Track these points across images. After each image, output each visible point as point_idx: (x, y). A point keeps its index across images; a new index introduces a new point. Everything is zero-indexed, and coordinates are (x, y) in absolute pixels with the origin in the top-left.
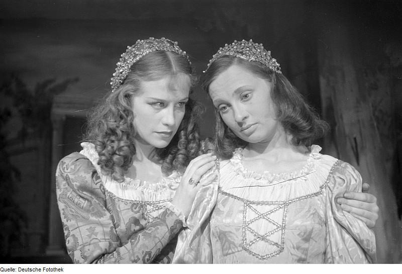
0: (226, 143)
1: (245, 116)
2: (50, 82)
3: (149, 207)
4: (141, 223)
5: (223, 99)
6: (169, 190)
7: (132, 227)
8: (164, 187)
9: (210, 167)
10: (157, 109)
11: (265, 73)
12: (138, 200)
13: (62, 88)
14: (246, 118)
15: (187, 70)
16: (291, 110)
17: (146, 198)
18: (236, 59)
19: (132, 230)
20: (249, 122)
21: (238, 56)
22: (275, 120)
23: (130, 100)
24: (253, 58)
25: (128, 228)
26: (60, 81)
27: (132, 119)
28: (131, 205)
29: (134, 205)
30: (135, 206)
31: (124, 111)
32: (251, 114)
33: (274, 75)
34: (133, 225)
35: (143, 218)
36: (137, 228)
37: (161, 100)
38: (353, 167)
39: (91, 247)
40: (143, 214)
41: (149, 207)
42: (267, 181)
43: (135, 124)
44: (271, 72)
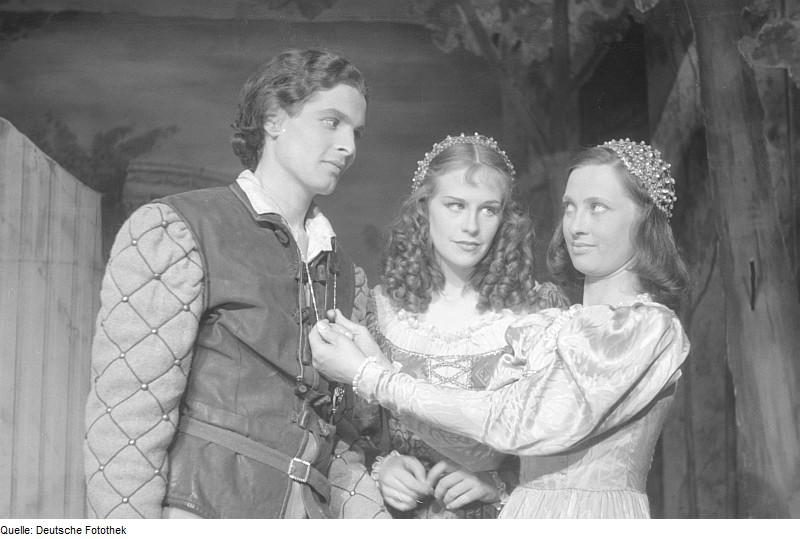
0: (558, 254)
1: (583, 230)
2: (123, 131)
10: (456, 212)
11: (641, 197)
13: (146, 143)
14: (582, 233)
16: (649, 263)
18: (617, 162)
20: (583, 240)
21: (623, 159)
23: (427, 208)
24: (638, 172)
26: (141, 131)
27: (428, 230)
31: (418, 220)
33: (651, 207)
37: (460, 200)
38: (49, 158)
42: (105, 317)
44: (648, 200)
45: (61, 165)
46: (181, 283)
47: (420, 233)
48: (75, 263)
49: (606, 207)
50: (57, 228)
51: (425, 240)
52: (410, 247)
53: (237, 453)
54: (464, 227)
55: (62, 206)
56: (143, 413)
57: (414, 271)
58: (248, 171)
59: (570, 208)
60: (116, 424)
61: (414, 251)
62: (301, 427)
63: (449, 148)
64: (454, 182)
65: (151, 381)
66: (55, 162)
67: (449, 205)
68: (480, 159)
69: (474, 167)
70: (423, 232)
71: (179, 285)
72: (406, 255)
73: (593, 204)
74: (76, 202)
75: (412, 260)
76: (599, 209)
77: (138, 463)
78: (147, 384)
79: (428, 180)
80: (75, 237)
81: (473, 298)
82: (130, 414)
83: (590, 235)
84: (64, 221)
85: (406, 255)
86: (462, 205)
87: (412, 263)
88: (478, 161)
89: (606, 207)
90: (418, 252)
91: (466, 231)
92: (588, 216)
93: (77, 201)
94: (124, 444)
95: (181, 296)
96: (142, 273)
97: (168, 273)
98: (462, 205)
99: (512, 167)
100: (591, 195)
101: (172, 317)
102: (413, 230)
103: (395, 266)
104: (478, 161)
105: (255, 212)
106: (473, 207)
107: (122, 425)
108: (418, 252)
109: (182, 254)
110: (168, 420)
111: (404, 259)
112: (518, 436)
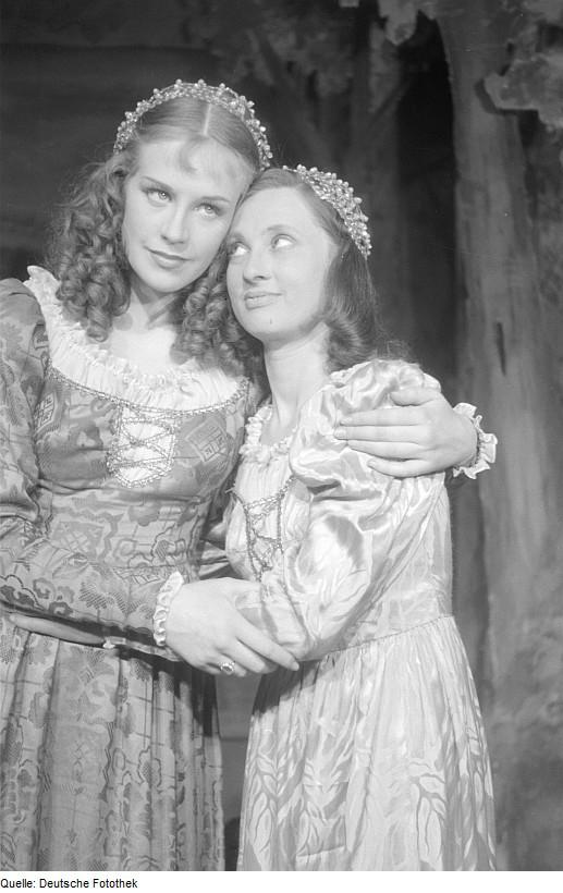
3: (126, 412)
4: (101, 437)
5: (288, 345)
6: (176, 393)
7: (80, 437)
8: (170, 384)
9: (390, 492)
12: (109, 392)
15: (227, 133)
17: (128, 395)
19: (80, 443)
22: (59, 305)
25: (73, 437)
27: (121, 220)
28: (92, 398)
29: (99, 399)
30: (100, 403)
32: (276, 277)
34: (83, 434)
35: (109, 428)
36: (91, 443)
39: (194, 346)
40: (111, 421)
41: (126, 412)
43: (330, 256)
47: (111, 224)
51: (119, 236)
52: (97, 242)
54: (164, 230)
57: (103, 280)
61: (103, 248)
63: (171, 100)
64: (161, 157)
67: (149, 191)
68: (209, 131)
69: (197, 139)
70: (115, 223)
72: (90, 251)
75: (101, 260)
76: (283, 243)
79: (130, 147)
81: (165, 336)
85: (90, 251)
86: (166, 192)
87: (100, 266)
88: (205, 132)
90: (109, 250)
91: (165, 238)
98: (166, 192)
99: (267, 148)
100: (273, 223)
102: (102, 217)
103: (73, 264)
104: (205, 132)
106: (183, 202)
108: (109, 250)
110: (247, 449)
111: (87, 256)
112: (285, 596)
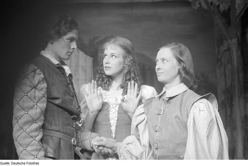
1: (160, 68)
14: (160, 69)
45: (81, 50)
46: (42, 89)
48: (86, 80)
49: (167, 61)
50: (80, 69)
53: (61, 139)
55: (81, 63)
56: (36, 130)
58: (43, 51)
59: (157, 62)
60: (28, 134)
62: (74, 128)
65: (37, 120)
66: (79, 50)
71: (42, 90)
73: (163, 60)
74: (85, 62)
76: (165, 61)
77: (38, 145)
78: (35, 121)
80: (85, 72)
82: (33, 131)
83: (162, 70)
84: (82, 67)
89: (167, 61)
92: (162, 64)
93: (86, 61)
94: (32, 140)
95: (42, 93)
96: (31, 87)
97: (39, 86)
100: (162, 57)
101: (40, 99)
105: (55, 64)
107: (30, 134)
109: (42, 79)
